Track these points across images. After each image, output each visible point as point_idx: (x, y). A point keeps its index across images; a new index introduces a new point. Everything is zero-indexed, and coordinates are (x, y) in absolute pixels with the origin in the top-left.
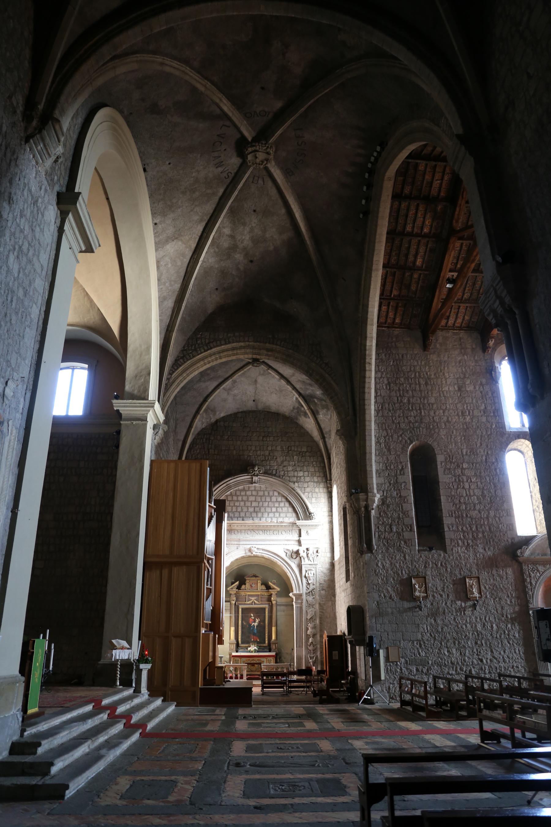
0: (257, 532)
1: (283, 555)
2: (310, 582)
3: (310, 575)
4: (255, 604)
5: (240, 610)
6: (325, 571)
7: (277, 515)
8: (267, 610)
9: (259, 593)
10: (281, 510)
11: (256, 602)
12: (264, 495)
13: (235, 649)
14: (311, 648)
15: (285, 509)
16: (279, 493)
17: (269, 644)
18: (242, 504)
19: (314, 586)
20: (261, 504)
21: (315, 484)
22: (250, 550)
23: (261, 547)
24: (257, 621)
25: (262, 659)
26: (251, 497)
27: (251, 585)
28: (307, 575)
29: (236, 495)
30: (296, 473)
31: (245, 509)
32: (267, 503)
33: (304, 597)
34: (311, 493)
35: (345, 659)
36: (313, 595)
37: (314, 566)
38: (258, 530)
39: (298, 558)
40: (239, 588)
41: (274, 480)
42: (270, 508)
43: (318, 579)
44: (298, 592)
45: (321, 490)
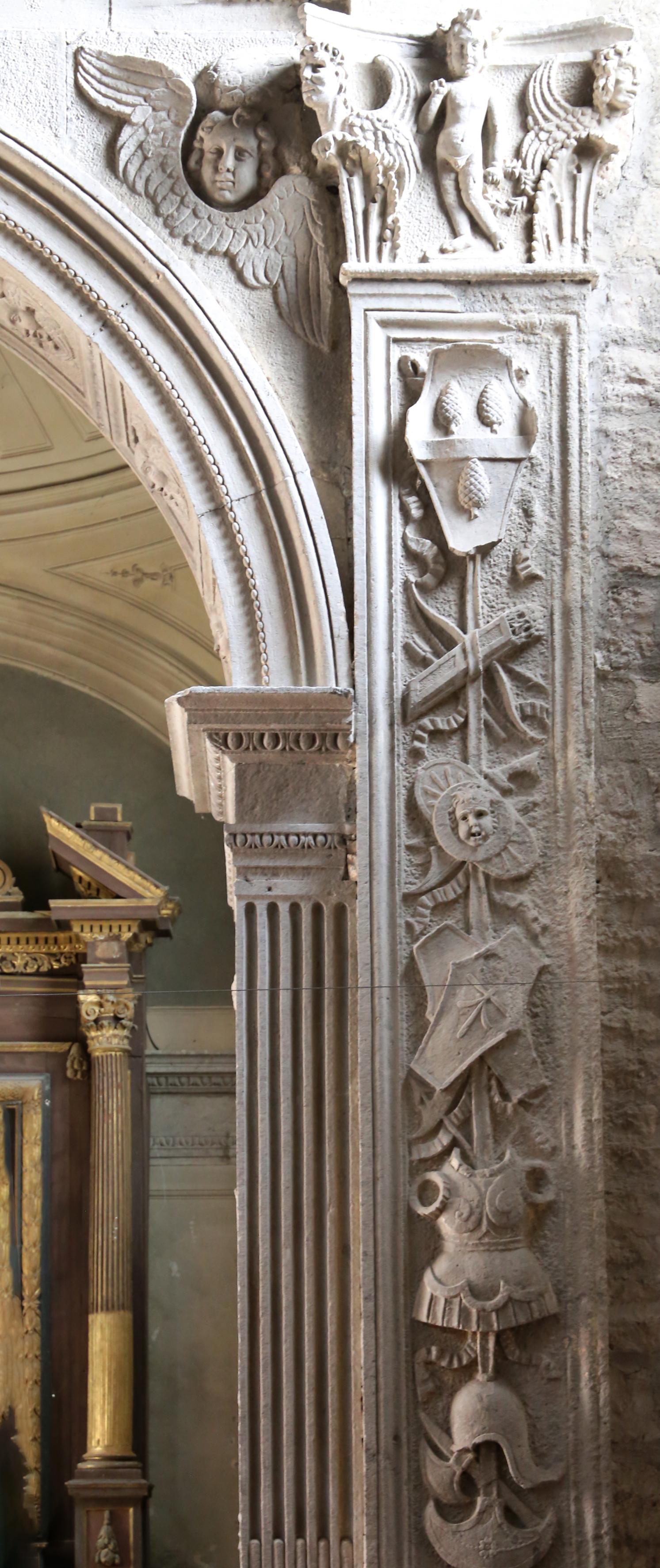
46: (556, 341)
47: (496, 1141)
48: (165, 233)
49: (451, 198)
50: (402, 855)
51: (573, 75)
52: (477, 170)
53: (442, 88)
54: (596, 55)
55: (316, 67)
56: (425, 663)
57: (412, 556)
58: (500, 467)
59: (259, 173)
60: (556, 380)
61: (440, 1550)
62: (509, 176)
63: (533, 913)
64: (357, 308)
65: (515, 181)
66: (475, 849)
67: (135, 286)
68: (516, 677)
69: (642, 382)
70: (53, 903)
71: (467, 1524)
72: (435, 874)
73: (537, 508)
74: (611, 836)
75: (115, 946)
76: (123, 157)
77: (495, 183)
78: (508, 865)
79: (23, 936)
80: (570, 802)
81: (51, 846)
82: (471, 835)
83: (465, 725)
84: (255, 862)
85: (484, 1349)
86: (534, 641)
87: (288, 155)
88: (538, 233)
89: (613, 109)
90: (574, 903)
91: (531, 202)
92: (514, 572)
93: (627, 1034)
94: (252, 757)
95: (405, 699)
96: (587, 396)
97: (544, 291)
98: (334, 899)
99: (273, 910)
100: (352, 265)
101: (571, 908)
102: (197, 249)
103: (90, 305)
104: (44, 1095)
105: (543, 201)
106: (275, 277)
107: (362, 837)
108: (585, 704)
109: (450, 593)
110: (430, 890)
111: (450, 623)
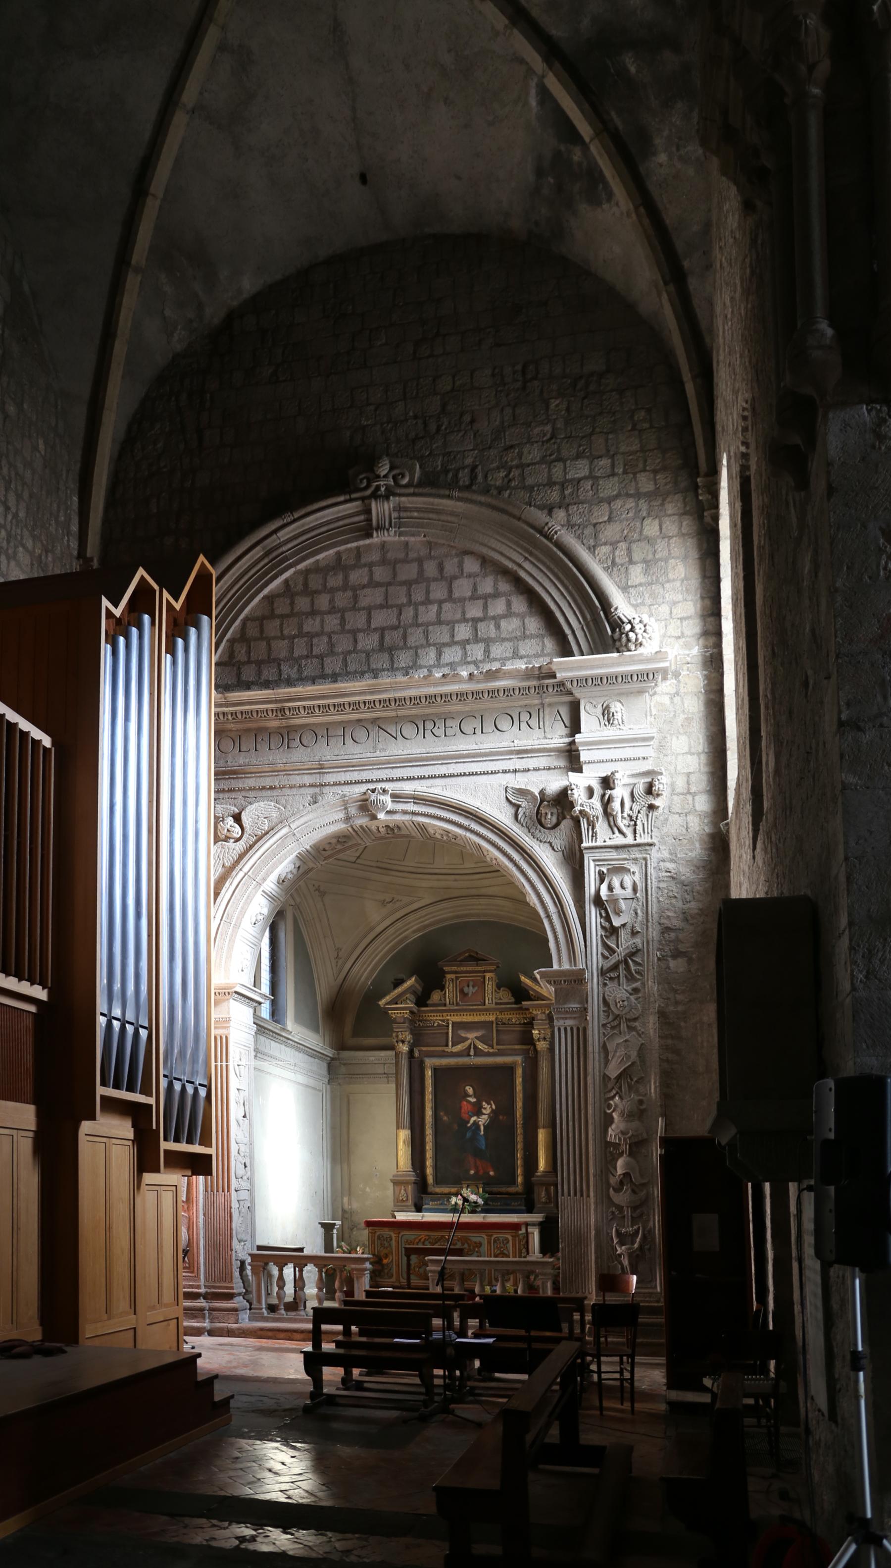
0: (392, 730)
1: (503, 816)
2: (617, 922)
3: (617, 890)
4: (478, 1053)
5: (429, 1073)
6: (686, 873)
7: (476, 651)
8: (519, 1072)
9: (491, 1018)
10: (493, 632)
11: (481, 1046)
12: (421, 576)
13: (410, 1203)
14: (622, 1198)
15: (510, 626)
16: (485, 561)
17: (529, 1186)
18: (332, 622)
19: (638, 940)
20: (408, 613)
21: (643, 505)
22: (366, 806)
23: (408, 788)
24: (487, 1109)
25: (476, 1237)
26: (367, 591)
27: (462, 991)
28: (604, 892)
29: (308, 592)
30: (557, 471)
31: (343, 644)
32: (434, 608)
33: (593, 984)
34: (623, 545)
35: (398, 1355)
36: (630, 978)
37: (636, 853)
38: (396, 720)
39: (566, 824)
40: (422, 1000)
41: (460, 507)
42: (445, 629)
43: (654, 908)
44: (566, 966)
45: (671, 526)
46: (644, 862)
47: (629, 1092)
48: (532, 837)
49: (612, 823)
50: (602, 1013)
51: (647, 785)
52: (619, 815)
53: (609, 792)
54: (653, 779)
55: (572, 790)
56: (607, 958)
57: (603, 927)
58: (628, 901)
59: (558, 819)
60: (644, 874)
61: (614, 1201)
62: (629, 815)
63: (640, 1028)
64: (586, 856)
65: (631, 817)
66: (622, 1011)
67: (525, 855)
68: (633, 961)
69: (670, 872)
70: (523, 1003)
71: (621, 1194)
72: (611, 1017)
73: (639, 912)
74: (663, 1005)
75: (544, 1015)
76: (520, 816)
77: (625, 818)
78: (632, 1014)
79: (515, 1012)
80: (649, 996)
81: (522, 985)
82: (620, 1007)
83: (619, 976)
84: (560, 1016)
85: (626, 1148)
86: (638, 951)
87: (566, 813)
88: (637, 832)
89: (658, 795)
90: (651, 1025)
91: (635, 822)
92: (632, 930)
93: (668, 1061)
94: (559, 986)
95: (602, 968)
96: (653, 878)
97: (640, 848)
98: (583, 1025)
99: (566, 1029)
100: (584, 845)
101: (650, 1027)
102: (541, 841)
103: (511, 860)
104: (522, 1062)
105: (639, 822)
106: (563, 848)
107: (590, 1009)
108: (653, 968)
109: (614, 937)
110: (609, 1023)
111: (614, 946)
